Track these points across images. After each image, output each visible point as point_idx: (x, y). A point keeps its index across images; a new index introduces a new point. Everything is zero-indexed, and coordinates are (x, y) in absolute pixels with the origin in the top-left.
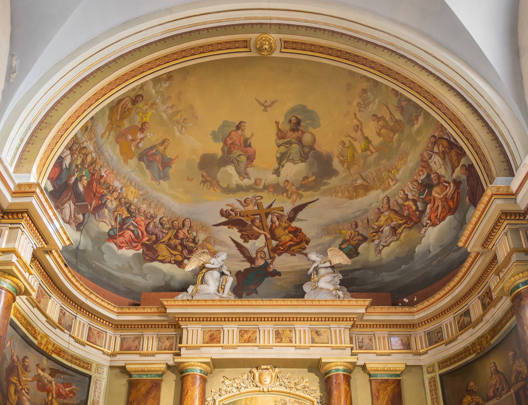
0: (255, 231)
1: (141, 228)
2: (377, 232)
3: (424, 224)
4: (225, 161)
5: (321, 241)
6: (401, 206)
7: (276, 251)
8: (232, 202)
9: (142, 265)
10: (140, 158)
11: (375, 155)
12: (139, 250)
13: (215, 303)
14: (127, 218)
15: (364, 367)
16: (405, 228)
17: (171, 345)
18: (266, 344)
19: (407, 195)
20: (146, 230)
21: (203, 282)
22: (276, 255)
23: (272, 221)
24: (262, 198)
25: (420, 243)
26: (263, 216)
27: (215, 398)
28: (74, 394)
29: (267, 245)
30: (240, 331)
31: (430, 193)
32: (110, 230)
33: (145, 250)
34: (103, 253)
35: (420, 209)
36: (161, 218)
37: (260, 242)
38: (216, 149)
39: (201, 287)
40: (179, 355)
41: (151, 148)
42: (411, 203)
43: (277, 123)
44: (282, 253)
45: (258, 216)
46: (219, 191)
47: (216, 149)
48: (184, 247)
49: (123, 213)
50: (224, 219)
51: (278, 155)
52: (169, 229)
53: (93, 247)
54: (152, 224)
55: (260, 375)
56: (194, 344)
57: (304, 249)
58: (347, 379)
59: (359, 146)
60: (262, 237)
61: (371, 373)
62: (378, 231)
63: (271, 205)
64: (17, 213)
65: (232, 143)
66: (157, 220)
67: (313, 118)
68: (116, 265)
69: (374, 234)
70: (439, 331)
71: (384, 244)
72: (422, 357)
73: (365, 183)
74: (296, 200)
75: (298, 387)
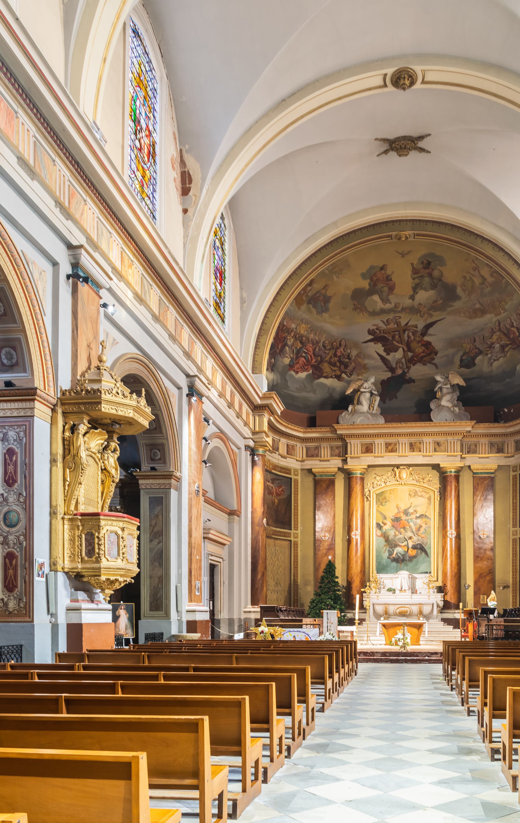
0: (395, 345)
2: (490, 347)
4: (371, 292)
6: (508, 330)
7: (411, 361)
8: (378, 322)
10: (309, 303)
11: (489, 289)
13: (369, 426)
14: (300, 348)
15: (469, 467)
16: (511, 348)
17: (340, 453)
19: (513, 323)
20: (314, 354)
21: (359, 403)
23: (408, 336)
24: (400, 317)
27: (370, 489)
28: (284, 492)
29: (404, 356)
30: (386, 444)
32: (290, 361)
34: (287, 381)
36: (323, 342)
37: (399, 354)
38: (365, 284)
39: (358, 407)
40: (345, 461)
42: (515, 330)
43: (412, 264)
45: (397, 333)
46: (366, 315)
47: (365, 284)
48: (341, 363)
49: (298, 345)
50: (371, 337)
51: (413, 285)
52: (330, 349)
53: (281, 379)
55: (399, 473)
57: (434, 359)
58: (457, 478)
59: (477, 281)
60: (401, 350)
61: (474, 471)
62: (491, 346)
63: (408, 323)
64: (262, 407)
65: (377, 279)
66: (321, 344)
67: (441, 261)
68: (296, 388)
69: (488, 349)
71: (495, 358)
73: (481, 307)
75: (425, 481)
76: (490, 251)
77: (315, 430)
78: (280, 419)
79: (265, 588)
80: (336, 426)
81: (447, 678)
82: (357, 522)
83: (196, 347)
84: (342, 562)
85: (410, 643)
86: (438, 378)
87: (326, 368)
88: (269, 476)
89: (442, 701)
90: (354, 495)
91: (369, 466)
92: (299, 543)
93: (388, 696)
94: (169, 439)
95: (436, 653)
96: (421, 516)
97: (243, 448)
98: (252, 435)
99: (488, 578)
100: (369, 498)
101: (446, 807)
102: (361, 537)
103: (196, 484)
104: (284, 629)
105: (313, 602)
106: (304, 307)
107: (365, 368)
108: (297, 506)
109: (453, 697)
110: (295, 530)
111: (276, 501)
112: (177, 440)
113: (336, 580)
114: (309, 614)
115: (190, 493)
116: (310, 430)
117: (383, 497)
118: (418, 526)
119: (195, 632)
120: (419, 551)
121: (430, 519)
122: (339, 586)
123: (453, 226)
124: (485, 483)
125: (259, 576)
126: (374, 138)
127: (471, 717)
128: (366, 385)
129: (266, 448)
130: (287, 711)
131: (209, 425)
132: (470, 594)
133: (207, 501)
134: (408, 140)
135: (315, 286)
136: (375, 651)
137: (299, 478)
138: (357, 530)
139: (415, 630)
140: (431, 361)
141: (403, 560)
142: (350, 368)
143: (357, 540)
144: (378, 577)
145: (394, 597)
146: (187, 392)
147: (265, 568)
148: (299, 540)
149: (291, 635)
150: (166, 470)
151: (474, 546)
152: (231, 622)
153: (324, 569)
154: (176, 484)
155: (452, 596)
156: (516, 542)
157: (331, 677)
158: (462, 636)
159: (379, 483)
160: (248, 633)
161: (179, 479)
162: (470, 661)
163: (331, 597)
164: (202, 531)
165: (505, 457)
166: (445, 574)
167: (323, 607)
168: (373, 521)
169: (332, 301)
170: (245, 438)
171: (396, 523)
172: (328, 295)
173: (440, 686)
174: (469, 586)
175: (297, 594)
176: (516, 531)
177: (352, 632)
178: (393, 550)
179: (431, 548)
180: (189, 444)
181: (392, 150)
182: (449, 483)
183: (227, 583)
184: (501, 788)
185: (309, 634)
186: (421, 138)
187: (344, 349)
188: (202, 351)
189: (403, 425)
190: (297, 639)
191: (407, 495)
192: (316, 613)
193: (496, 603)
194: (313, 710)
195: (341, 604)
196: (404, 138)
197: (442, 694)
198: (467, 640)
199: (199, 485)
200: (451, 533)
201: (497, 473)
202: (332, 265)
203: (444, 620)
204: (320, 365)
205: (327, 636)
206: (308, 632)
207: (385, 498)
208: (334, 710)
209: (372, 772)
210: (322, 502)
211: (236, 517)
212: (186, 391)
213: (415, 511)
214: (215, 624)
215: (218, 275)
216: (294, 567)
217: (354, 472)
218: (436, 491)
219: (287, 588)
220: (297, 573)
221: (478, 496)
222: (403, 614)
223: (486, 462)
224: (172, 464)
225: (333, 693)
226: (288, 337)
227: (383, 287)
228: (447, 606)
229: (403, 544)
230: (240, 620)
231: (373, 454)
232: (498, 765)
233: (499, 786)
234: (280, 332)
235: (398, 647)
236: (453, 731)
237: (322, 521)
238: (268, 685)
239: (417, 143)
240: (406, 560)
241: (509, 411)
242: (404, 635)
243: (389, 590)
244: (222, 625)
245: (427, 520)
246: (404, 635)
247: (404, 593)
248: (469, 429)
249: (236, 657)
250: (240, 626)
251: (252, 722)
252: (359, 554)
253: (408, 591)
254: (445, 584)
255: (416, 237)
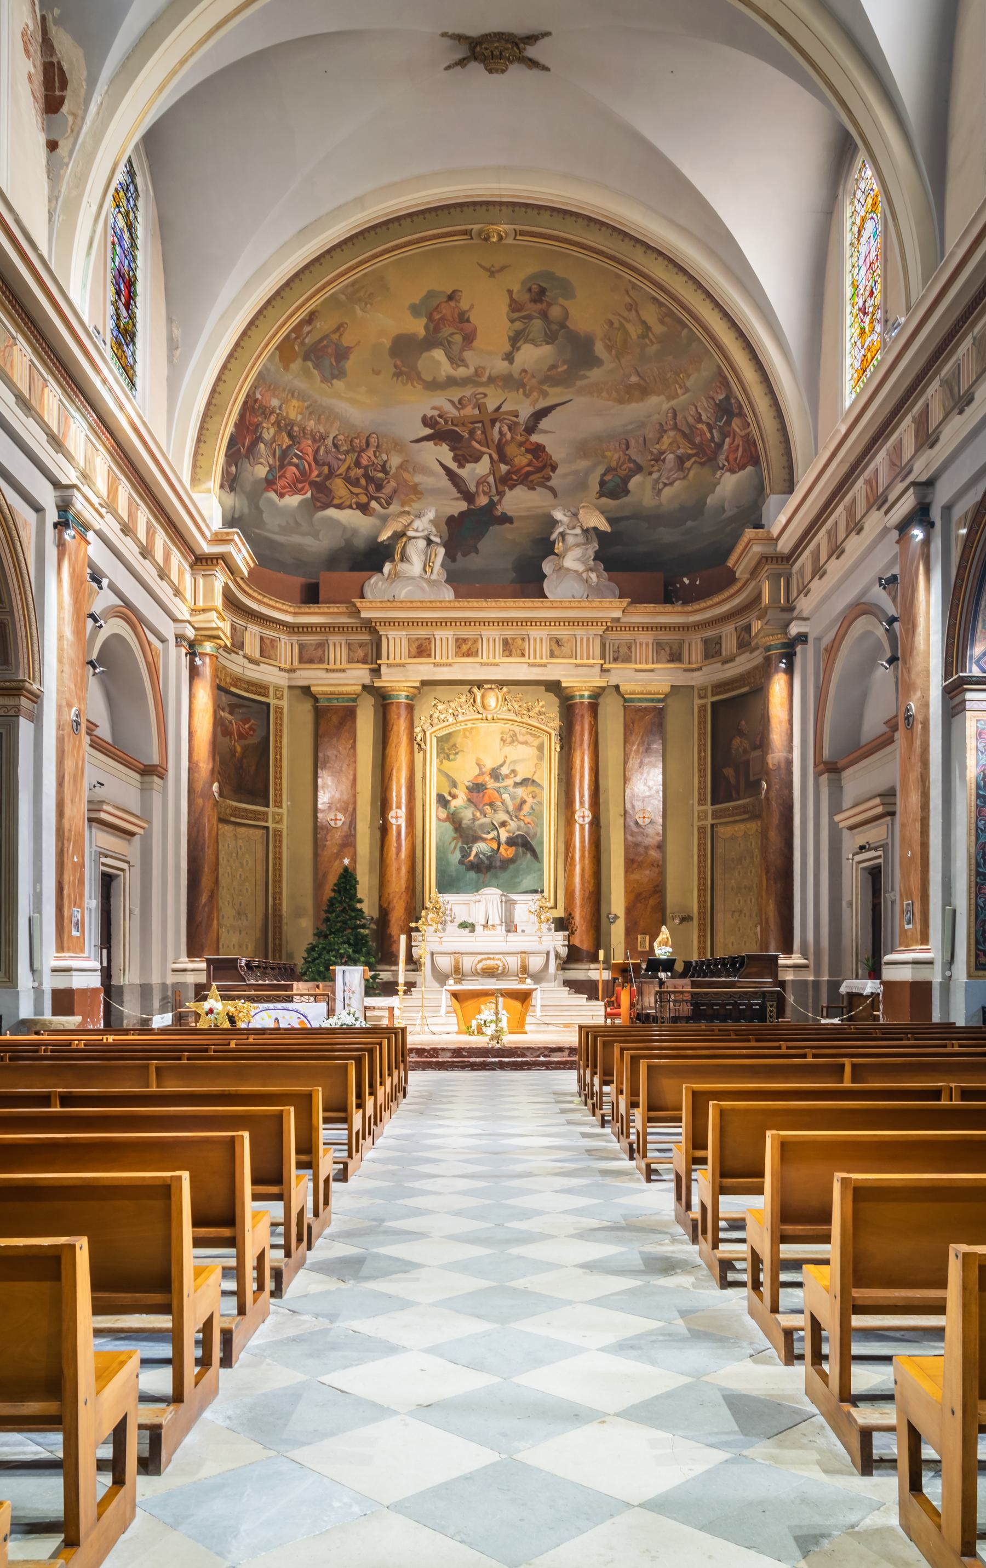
1: (307, 457)
2: (656, 460)
3: (721, 465)
4: (430, 342)
5: (574, 467)
7: (506, 482)
8: (441, 403)
9: (312, 516)
10: (306, 358)
12: (305, 493)
14: (289, 447)
15: (617, 687)
16: (695, 462)
17: (366, 655)
18: (491, 660)
19: (700, 415)
20: (315, 460)
21: (404, 558)
22: (506, 488)
23: (500, 432)
24: (485, 395)
25: (713, 492)
26: (488, 424)
27: (425, 727)
28: (254, 731)
29: (493, 472)
30: (457, 640)
31: (729, 423)
33: (315, 492)
34: (260, 512)
35: (716, 440)
36: (335, 437)
37: (482, 467)
38: (418, 327)
39: (402, 567)
40: (376, 672)
41: (321, 340)
42: (705, 428)
43: (510, 292)
44: (515, 486)
45: (480, 425)
46: (419, 387)
47: (418, 327)
48: (370, 479)
49: (283, 442)
50: (428, 431)
51: (512, 334)
52: (347, 452)
53: (250, 507)
54: (322, 448)
55: (483, 697)
56: (398, 661)
57: (549, 479)
58: (594, 708)
59: (634, 331)
60: (486, 458)
61: (626, 696)
62: (658, 458)
63: (500, 407)
64: (212, 559)
65: (441, 319)
66: (329, 441)
68: (279, 525)
69: (653, 462)
70: (718, 641)
72: (696, 674)
73: (642, 382)
74: (537, 400)
75: (532, 714)
76: (660, 272)
77: (317, 610)
78: (248, 585)
79: (215, 921)
80: (357, 601)
81: (590, 1102)
82: (399, 792)
83: (73, 427)
84: (371, 871)
85: (506, 1029)
86: (558, 515)
87: (339, 488)
88: (224, 698)
89: (587, 1151)
90: (393, 739)
91: (424, 683)
92: (284, 833)
93: (475, 1142)
94: (16, 615)
95: (560, 1049)
96: (525, 782)
97: (172, 641)
98: (191, 615)
99: (652, 902)
100: (423, 746)
101: (648, 1413)
102: (407, 821)
103: (74, 709)
104: (256, 1005)
105: (311, 949)
106: (296, 366)
107: (416, 491)
108: (281, 759)
109: (608, 1141)
110: (275, 806)
111: (239, 749)
112: (33, 616)
113: (359, 906)
114: (305, 974)
115: (60, 727)
116: (307, 610)
117: (451, 743)
118: (518, 801)
119: (71, 1013)
120: (520, 850)
121: (543, 788)
122: (364, 918)
123: (590, 219)
124: (647, 720)
125: (204, 899)
126: (440, 32)
127: (652, 1184)
128: (417, 524)
129: (219, 641)
130: (274, 1189)
131: (101, 588)
132: (617, 932)
133: (97, 745)
134: (507, 41)
135: (318, 326)
136: (439, 1047)
137: (285, 704)
138: (399, 807)
139: (517, 1004)
140: (544, 483)
141: (489, 868)
142: (388, 490)
143: (399, 827)
144: (441, 899)
145: (473, 939)
146: (56, 519)
147: (217, 882)
148: (284, 826)
149: (270, 1017)
150: (8, 677)
151: (625, 839)
152: (145, 991)
153: (335, 885)
154: (31, 708)
155: (584, 937)
156: (705, 833)
157: (360, 1106)
158: (607, 1015)
159: (442, 717)
160: (180, 1013)
161: (37, 697)
162: (650, 1068)
163: (349, 939)
164: (85, 806)
165: (686, 670)
166: (569, 894)
167: (333, 959)
168: (432, 787)
169: (352, 357)
170: (175, 620)
171: (475, 794)
172: (346, 344)
173: (577, 1116)
174: (616, 917)
175: (280, 933)
176: (706, 812)
177: (391, 1010)
178: (470, 848)
179: (542, 843)
180: (59, 626)
181: (476, 59)
182: (579, 718)
183: (137, 911)
184: (758, 1356)
185: (306, 1013)
186: (532, 39)
187: (374, 452)
188: (87, 436)
189: (489, 605)
190: (281, 1026)
191: (498, 740)
192: (319, 973)
193: (671, 950)
194: (327, 1181)
195: (368, 954)
196: (500, 36)
197: (584, 1135)
198: (617, 1021)
199: (79, 710)
200: (583, 814)
201: (669, 701)
202: (353, 284)
203: (568, 983)
204: (327, 483)
205: (343, 1018)
206: (303, 1011)
207: (454, 745)
208: (368, 1176)
209: (471, 1327)
210: (331, 753)
211: (156, 779)
212: (52, 515)
213: (513, 771)
214: (113, 994)
215: (122, 287)
216: (275, 881)
217: (395, 693)
218: (553, 733)
219: (259, 924)
220: (280, 893)
221: (633, 745)
222: (490, 973)
223: (646, 678)
224: (21, 665)
225: (364, 1138)
226: (264, 425)
227: (453, 334)
228: (573, 956)
229: (489, 836)
230: (164, 986)
231: (431, 660)
232: (738, 1299)
233: (752, 1352)
234: (248, 414)
235: (486, 1039)
236: (625, 1217)
237: (329, 792)
238: (233, 1137)
239: (525, 49)
240: (495, 868)
241: (692, 582)
242: (497, 1014)
243: (463, 925)
244: (127, 997)
245: (537, 790)
246: (497, 1014)
247: (492, 932)
248: (617, 614)
249: (157, 1068)
250: (164, 998)
251: (196, 1223)
252: (403, 855)
253: (499, 927)
254: (570, 914)
255: (518, 237)
